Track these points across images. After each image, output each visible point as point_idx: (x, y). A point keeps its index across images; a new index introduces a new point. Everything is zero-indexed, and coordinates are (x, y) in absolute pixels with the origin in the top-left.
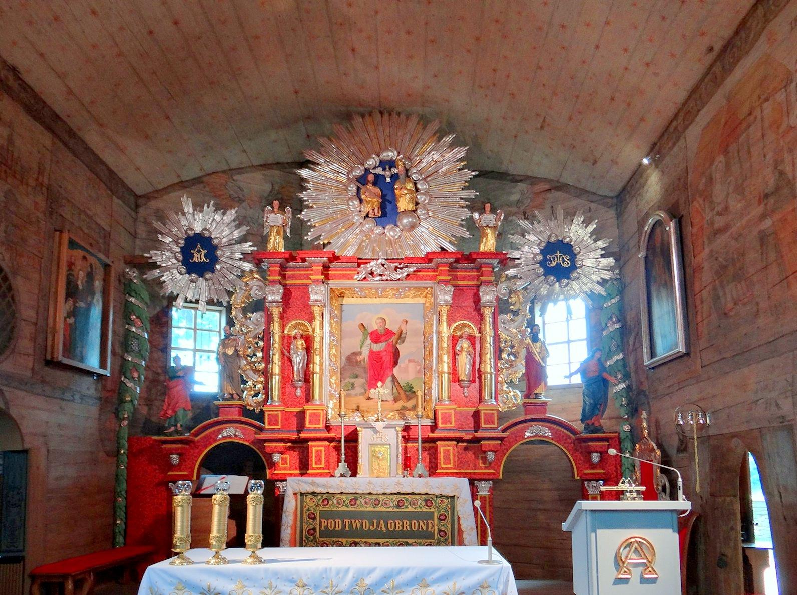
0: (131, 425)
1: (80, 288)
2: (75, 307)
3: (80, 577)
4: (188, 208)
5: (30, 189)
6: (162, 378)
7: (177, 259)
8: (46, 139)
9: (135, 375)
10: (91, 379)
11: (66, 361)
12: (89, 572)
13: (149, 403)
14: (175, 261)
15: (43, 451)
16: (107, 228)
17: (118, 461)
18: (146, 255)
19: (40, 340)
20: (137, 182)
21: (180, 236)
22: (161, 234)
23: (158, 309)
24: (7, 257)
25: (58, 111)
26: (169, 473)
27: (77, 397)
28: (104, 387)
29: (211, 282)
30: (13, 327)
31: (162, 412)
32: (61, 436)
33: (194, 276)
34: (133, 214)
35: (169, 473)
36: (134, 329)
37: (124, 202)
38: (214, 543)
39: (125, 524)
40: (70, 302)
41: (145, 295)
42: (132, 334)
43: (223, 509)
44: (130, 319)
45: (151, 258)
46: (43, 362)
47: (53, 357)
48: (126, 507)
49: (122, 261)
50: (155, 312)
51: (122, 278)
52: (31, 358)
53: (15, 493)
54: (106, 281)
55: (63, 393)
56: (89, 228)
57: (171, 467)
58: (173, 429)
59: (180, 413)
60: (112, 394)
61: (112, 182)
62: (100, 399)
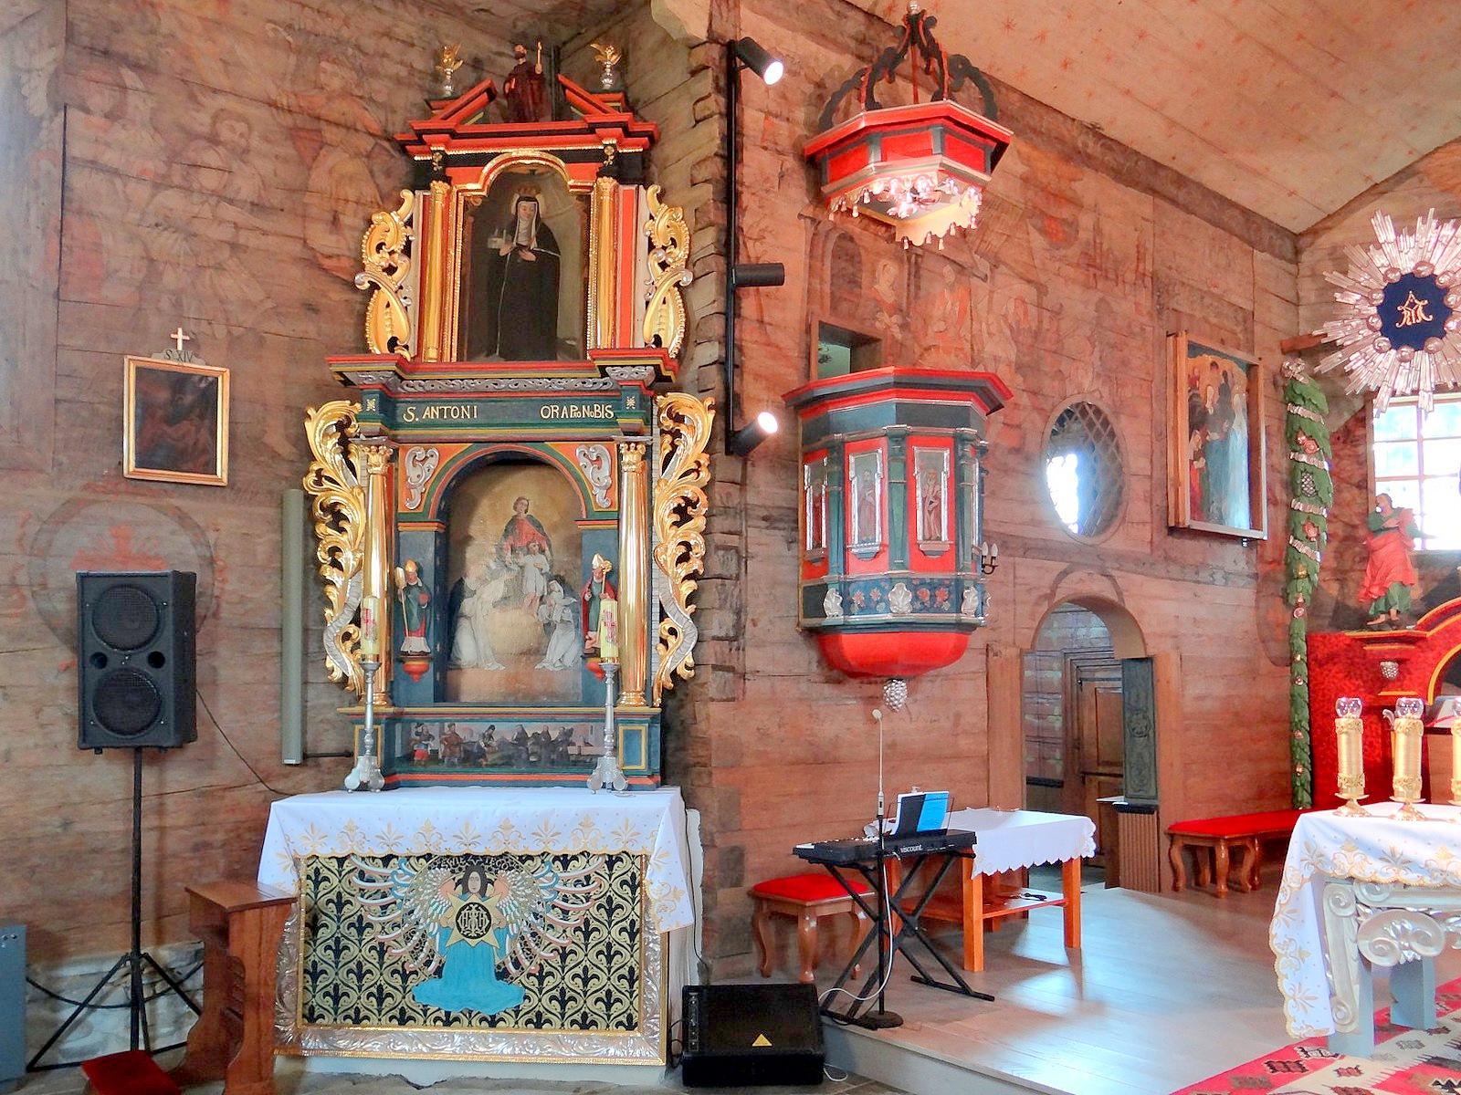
0: (1314, 610)
1: (1211, 412)
2: (1205, 443)
3: (1238, 843)
4: (1386, 233)
5: (1127, 287)
6: (1361, 532)
7: (1371, 328)
8: (1142, 204)
9: (1312, 533)
10: (1238, 546)
11: (1197, 525)
12: (1252, 839)
13: (1339, 576)
14: (1366, 332)
15: (1174, 658)
16: (1248, 306)
17: (1292, 673)
18: (1316, 333)
19: (1158, 499)
20: (1295, 216)
21: (1375, 285)
22: (1342, 290)
23: (1347, 416)
24: (1106, 395)
25: (1155, 155)
26: (1382, 693)
27: (1218, 576)
28: (1260, 558)
29: (1439, 355)
30: (1121, 488)
31: (1364, 591)
32: (1200, 636)
33: (1406, 350)
34: (1292, 268)
35: (1382, 693)
36: (1304, 458)
37: (1272, 254)
38: (1401, 789)
39: (1312, 773)
40: (1197, 436)
41: (1320, 399)
42: (1302, 467)
43: (1412, 739)
44: (1297, 443)
45: (1325, 335)
46: (1166, 531)
47: (1177, 523)
48: (1311, 747)
49: (1278, 351)
50: (1342, 423)
51: (1279, 378)
52: (1148, 527)
53: (1140, 716)
54: (1251, 391)
55: (1197, 573)
56: (1218, 315)
57: (1384, 682)
58: (1383, 618)
59: (1395, 590)
60: (1276, 569)
61: (1250, 228)
62: (1256, 576)
